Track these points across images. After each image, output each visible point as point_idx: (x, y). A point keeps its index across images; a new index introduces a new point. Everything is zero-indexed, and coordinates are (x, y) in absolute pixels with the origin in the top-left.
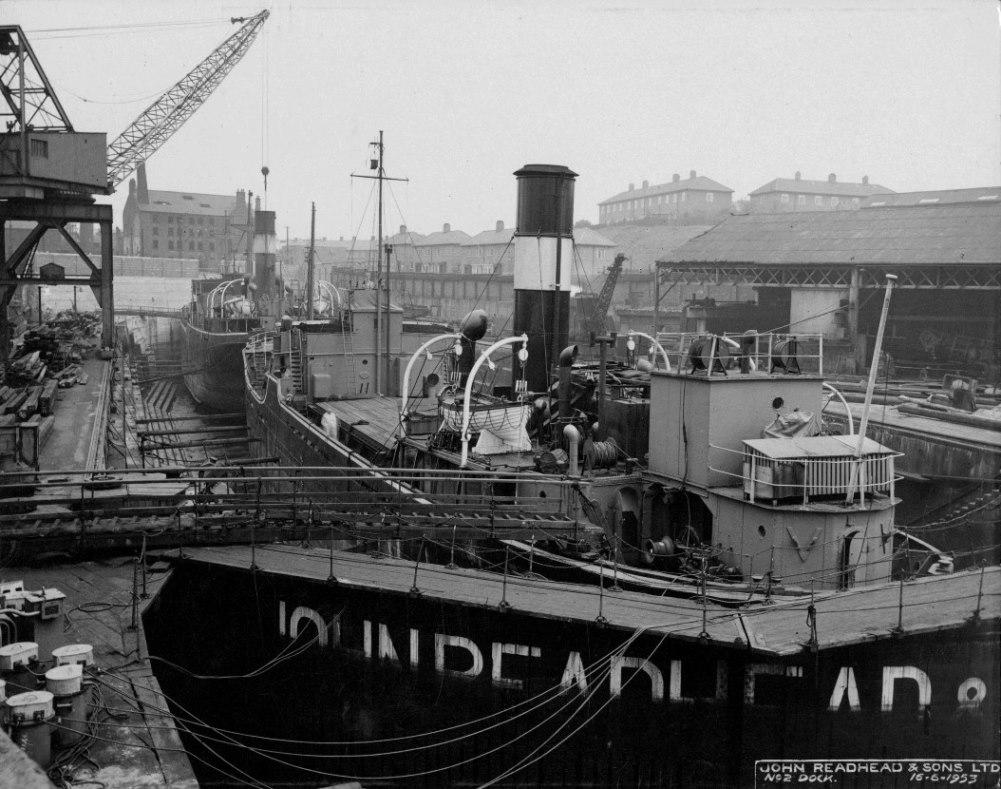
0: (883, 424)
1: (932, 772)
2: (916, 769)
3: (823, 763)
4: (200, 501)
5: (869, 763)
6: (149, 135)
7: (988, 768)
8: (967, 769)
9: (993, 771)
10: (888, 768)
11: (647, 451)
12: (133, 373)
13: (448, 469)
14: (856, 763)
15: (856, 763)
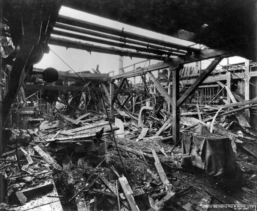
0: (122, 54)
1: (239, 207)
2: (235, 207)
3: (216, 206)
4: (95, 154)
5: (225, 206)
6: (228, 64)
7: (251, 207)
8: (246, 207)
9: (252, 207)
10: (229, 207)
11: (227, 93)
12: (196, 194)
13: (157, 44)
14: (223, 206)
15: (223, 206)
